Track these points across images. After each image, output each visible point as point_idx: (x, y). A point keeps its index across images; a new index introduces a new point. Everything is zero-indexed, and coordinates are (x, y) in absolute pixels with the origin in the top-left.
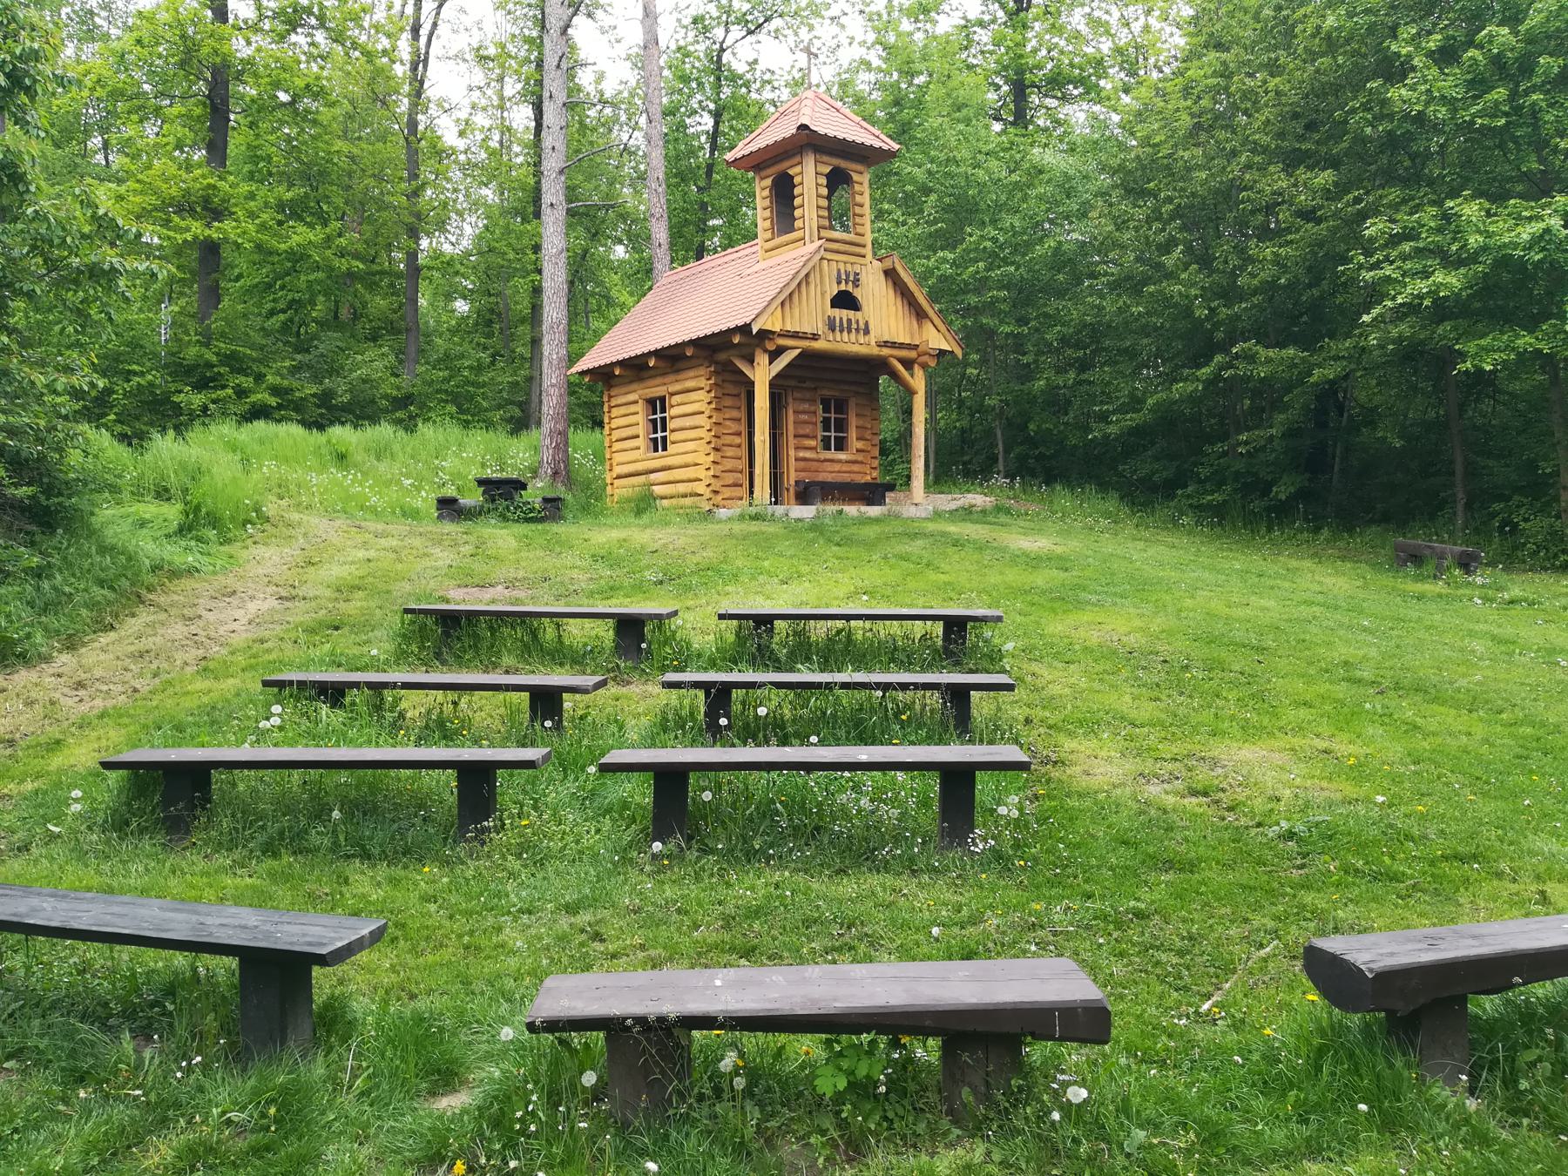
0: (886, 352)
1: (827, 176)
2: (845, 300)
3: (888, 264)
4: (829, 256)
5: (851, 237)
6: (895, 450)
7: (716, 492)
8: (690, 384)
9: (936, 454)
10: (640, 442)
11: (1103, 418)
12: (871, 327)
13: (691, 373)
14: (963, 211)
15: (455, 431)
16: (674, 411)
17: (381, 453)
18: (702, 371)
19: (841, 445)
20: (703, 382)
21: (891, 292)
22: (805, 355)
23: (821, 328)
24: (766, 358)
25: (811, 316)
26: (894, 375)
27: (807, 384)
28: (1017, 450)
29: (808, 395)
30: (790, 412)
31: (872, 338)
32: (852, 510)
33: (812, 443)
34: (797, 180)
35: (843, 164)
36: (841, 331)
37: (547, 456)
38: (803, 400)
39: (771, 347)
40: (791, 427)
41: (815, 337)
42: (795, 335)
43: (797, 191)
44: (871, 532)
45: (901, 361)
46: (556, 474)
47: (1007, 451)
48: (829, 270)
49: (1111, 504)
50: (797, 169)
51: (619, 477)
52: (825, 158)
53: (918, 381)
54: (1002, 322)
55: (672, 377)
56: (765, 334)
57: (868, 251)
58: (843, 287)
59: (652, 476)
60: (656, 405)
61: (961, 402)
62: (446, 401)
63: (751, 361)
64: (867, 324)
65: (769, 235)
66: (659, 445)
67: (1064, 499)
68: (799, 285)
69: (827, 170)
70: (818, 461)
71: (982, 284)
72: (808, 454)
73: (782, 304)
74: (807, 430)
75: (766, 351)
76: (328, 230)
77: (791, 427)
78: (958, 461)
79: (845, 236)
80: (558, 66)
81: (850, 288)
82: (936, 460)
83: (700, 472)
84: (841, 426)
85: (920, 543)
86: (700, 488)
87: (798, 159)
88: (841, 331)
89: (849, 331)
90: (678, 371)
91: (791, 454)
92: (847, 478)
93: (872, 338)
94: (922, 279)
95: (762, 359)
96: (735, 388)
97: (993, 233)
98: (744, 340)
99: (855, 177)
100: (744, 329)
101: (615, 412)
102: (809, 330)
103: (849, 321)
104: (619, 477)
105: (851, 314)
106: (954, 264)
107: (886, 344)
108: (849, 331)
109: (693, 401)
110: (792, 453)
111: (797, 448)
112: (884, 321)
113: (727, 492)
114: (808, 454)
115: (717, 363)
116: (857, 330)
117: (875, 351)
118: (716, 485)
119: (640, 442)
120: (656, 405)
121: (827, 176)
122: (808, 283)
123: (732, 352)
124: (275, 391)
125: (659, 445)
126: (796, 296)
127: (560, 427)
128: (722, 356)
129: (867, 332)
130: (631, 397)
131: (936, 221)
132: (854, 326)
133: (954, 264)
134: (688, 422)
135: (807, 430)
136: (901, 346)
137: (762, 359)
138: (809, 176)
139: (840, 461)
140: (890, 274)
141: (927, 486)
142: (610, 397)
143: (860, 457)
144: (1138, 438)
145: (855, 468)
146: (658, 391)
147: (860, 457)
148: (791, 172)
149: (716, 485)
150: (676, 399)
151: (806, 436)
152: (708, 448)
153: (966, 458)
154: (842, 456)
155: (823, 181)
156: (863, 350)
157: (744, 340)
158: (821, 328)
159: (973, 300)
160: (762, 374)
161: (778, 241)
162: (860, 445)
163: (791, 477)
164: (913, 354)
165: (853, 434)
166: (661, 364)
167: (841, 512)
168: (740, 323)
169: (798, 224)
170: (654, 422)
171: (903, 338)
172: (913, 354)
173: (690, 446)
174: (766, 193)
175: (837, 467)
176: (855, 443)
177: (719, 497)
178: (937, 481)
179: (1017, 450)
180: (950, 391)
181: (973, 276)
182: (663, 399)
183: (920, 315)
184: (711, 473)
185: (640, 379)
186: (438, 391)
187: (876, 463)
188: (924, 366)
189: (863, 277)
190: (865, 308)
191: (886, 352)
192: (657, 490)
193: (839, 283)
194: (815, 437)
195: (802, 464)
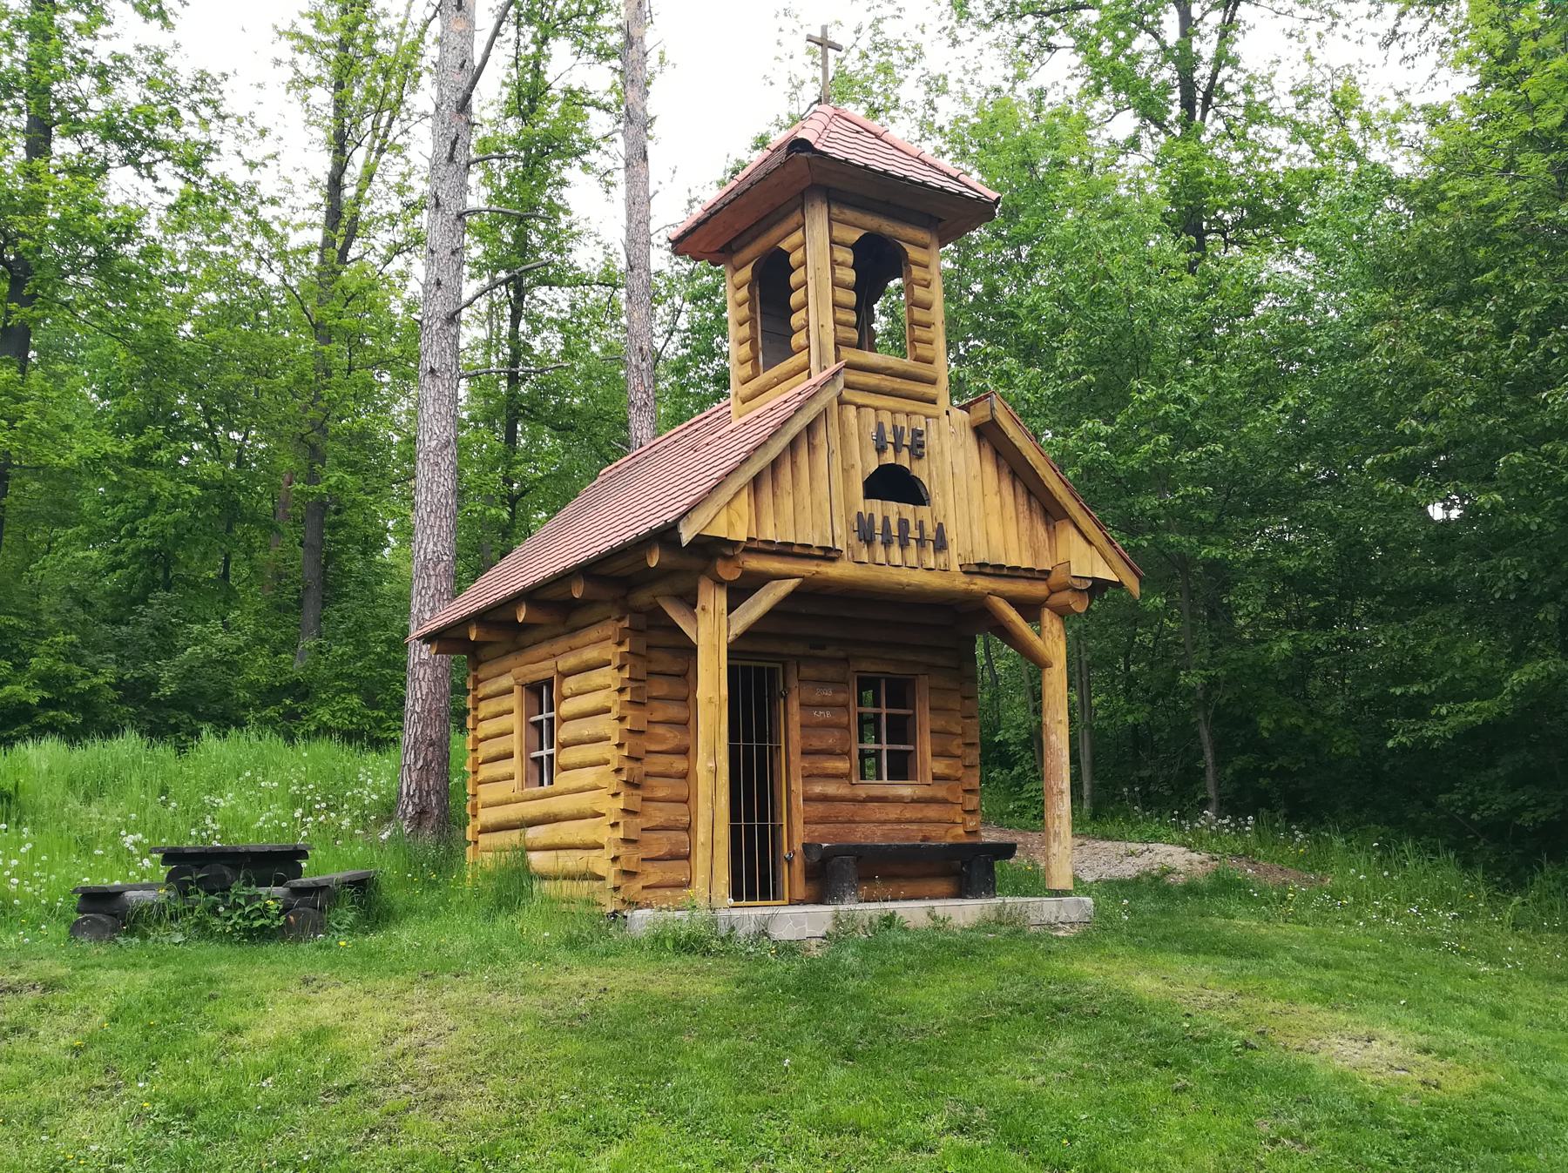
0: (981, 584)
1: (856, 248)
2: (894, 484)
3: (981, 413)
4: (860, 398)
5: (907, 364)
6: (1009, 763)
7: (629, 874)
8: (591, 654)
9: (1094, 763)
10: (514, 766)
11: (1417, 709)
12: (951, 534)
13: (593, 633)
14: (1117, 364)
15: (273, 744)
16: (567, 708)
17: (95, 789)
18: (610, 628)
19: (901, 768)
20: (611, 651)
21: (990, 469)
22: (810, 594)
23: (842, 538)
24: (722, 600)
25: (818, 510)
26: (1004, 632)
27: (829, 652)
28: (1239, 762)
29: (831, 672)
30: (794, 706)
31: (953, 558)
32: (913, 912)
33: (842, 765)
34: (795, 258)
35: (888, 227)
36: (887, 543)
37: (408, 783)
38: (822, 682)
39: (729, 573)
40: (795, 734)
41: (829, 554)
42: (785, 550)
43: (794, 279)
44: (939, 997)
45: (1014, 602)
46: (421, 814)
47: (1220, 763)
48: (859, 425)
49: (1448, 874)
50: (796, 238)
51: (485, 830)
52: (850, 214)
53: (1052, 642)
54: (1203, 542)
55: (562, 644)
56: (711, 549)
57: (942, 391)
58: (889, 458)
59: (536, 834)
60: (539, 692)
61: (1131, 680)
62: (349, 691)
63: (689, 601)
64: (940, 530)
65: (747, 370)
66: (542, 770)
67: (1352, 869)
68: (793, 445)
69: (854, 235)
70: (854, 800)
71: (1160, 478)
72: (832, 789)
73: (756, 482)
74: (831, 740)
75: (719, 582)
76: (142, 439)
77: (795, 734)
78: (1131, 779)
79: (893, 361)
80: (451, 159)
81: (904, 460)
82: (1094, 774)
83: (605, 834)
84: (901, 730)
85: (1064, 1045)
86: (600, 863)
87: (796, 218)
88: (887, 543)
89: (904, 545)
90: (574, 630)
91: (796, 791)
92: (912, 835)
93: (953, 558)
94: (1060, 465)
95: (713, 600)
96: (662, 659)
97: (1179, 389)
98: (672, 560)
99: (913, 253)
100: (665, 535)
101: (486, 708)
102: (815, 539)
103: (903, 523)
104: (485, 830)
105: (907, 510)
106: (1113, 442)
107: (982, 569)
108: (904, 545)
109: (595, 685)
110: (798, 786)
111: (809, 777)
112: (976, 523)
113: (654, 873)
114: (832, 789)
115: (636, 611)
116: (921, 542)
117: (960, 583)
118: (632, 857)
119: (514, 766)
120: (539, 692)
121: (856, 248)
122: (812, 448)
123: (660, 588)
124: (45, 680)
125: (542, 770)
126: (786, 471)
127: (432, 733)
128: (642, 598)
129: (941, 545)
130: (506, 682)
131: (1077, 375)
132: (914, 533)
133: (1113, 442)
134: (585, 728)
135: (831, 740)
136: (1015, 573)
137: (713, 600)
138: (819, 250)
139: (899, 800)
140: (987, 433)
141: (1077, 823)
142: (477, 681)
143: (941, 791)
144: (1481, 743)
145: (932, 812)
146: (543, 670)
147: (941, 791)
148: (784, 246)
149: (632, 857)
150: (570, 684)
151: (829, 753)
152: (614, 783)
153: (1145, 773)
154: (905, 790)
155: (847, 256)
156: (935, 581)
157: (672, 560)
158: (842, 538)
159: (1150, 502)
160: (713, 629)
161: (765, 377)
162: (940, 767)
163: (797, 832)
164: (1039, 589)
165: (925, 745)
166: (538, 617)
167: (889, 921)
168: (656, 523)
169: (797, 340)
170: (538, 725)
171: (1017, 557)
172: (1039, 589)
173: (588, 776)
174: (744, 293)
175: (893, 812)
176: (929, 763)
177: (637, 885)
178: (1094, 817)
179: (1239, 762)
180: (1111, 663)
181: (1147, 461)
182: (549, 683)
183: (1050, 512)
184: (620, 833)
185: (519, 648)
186: (338, 677)
187: (973, 802)
188: (1063, 613)
189: (931, 440)
190: (936, 499)
191: (981, 584)
192: (538, 860)
193: (881, 450)
194: (848, 753)
195: (819, 809)
